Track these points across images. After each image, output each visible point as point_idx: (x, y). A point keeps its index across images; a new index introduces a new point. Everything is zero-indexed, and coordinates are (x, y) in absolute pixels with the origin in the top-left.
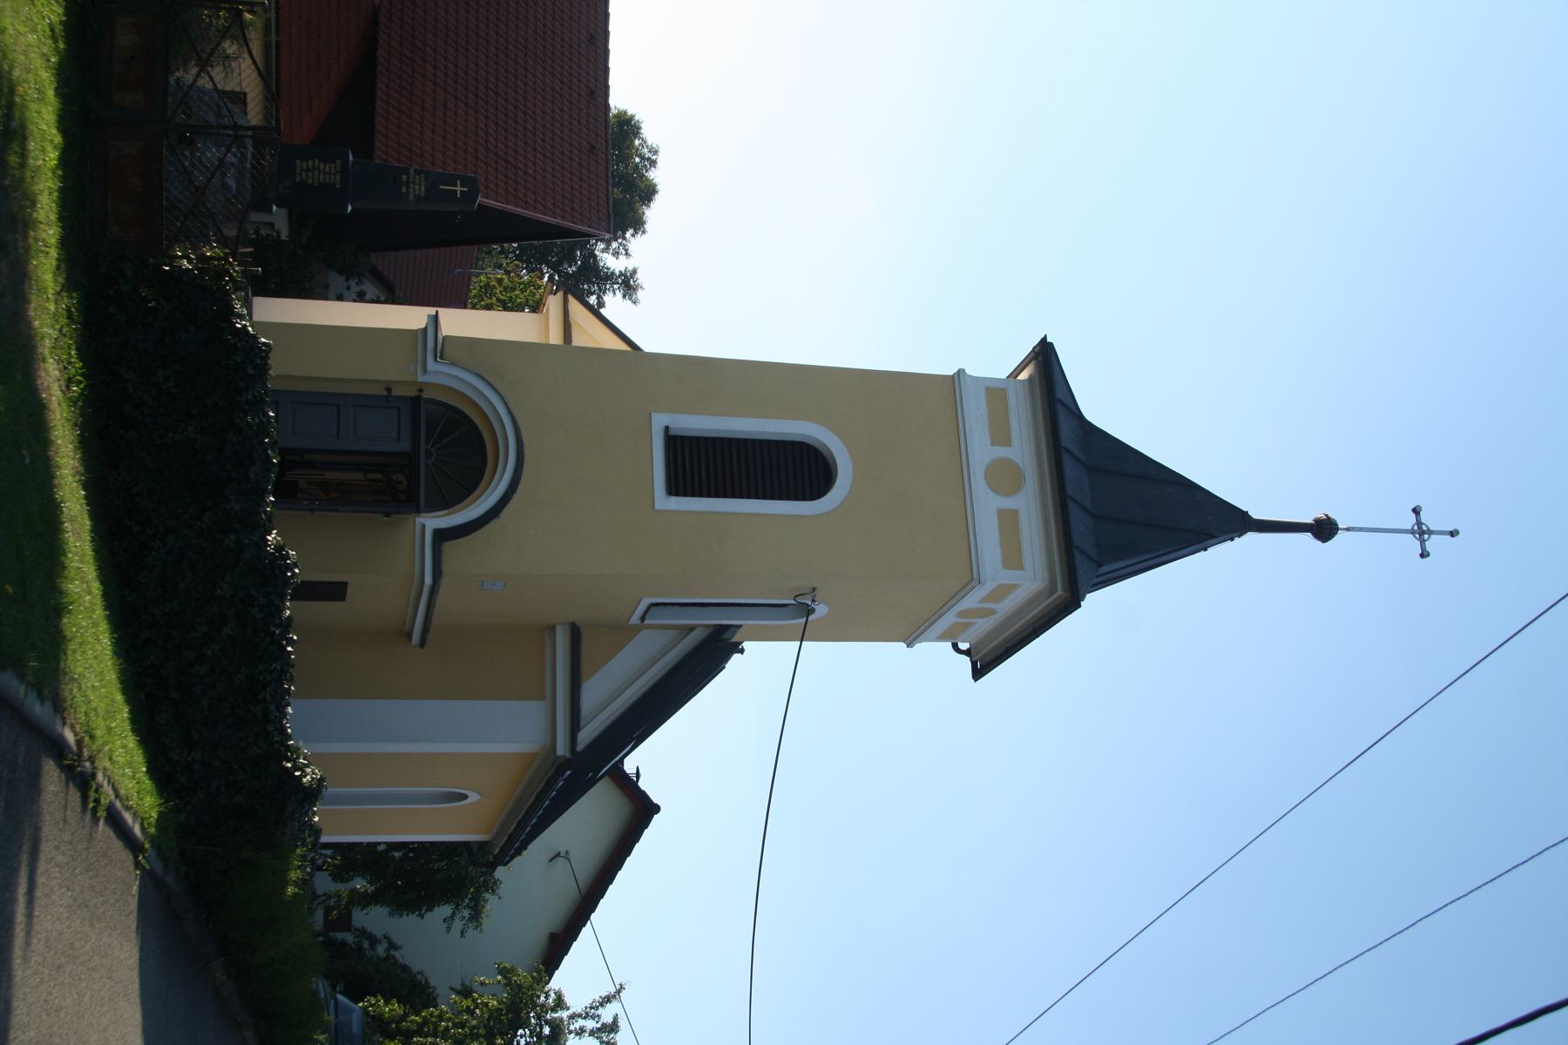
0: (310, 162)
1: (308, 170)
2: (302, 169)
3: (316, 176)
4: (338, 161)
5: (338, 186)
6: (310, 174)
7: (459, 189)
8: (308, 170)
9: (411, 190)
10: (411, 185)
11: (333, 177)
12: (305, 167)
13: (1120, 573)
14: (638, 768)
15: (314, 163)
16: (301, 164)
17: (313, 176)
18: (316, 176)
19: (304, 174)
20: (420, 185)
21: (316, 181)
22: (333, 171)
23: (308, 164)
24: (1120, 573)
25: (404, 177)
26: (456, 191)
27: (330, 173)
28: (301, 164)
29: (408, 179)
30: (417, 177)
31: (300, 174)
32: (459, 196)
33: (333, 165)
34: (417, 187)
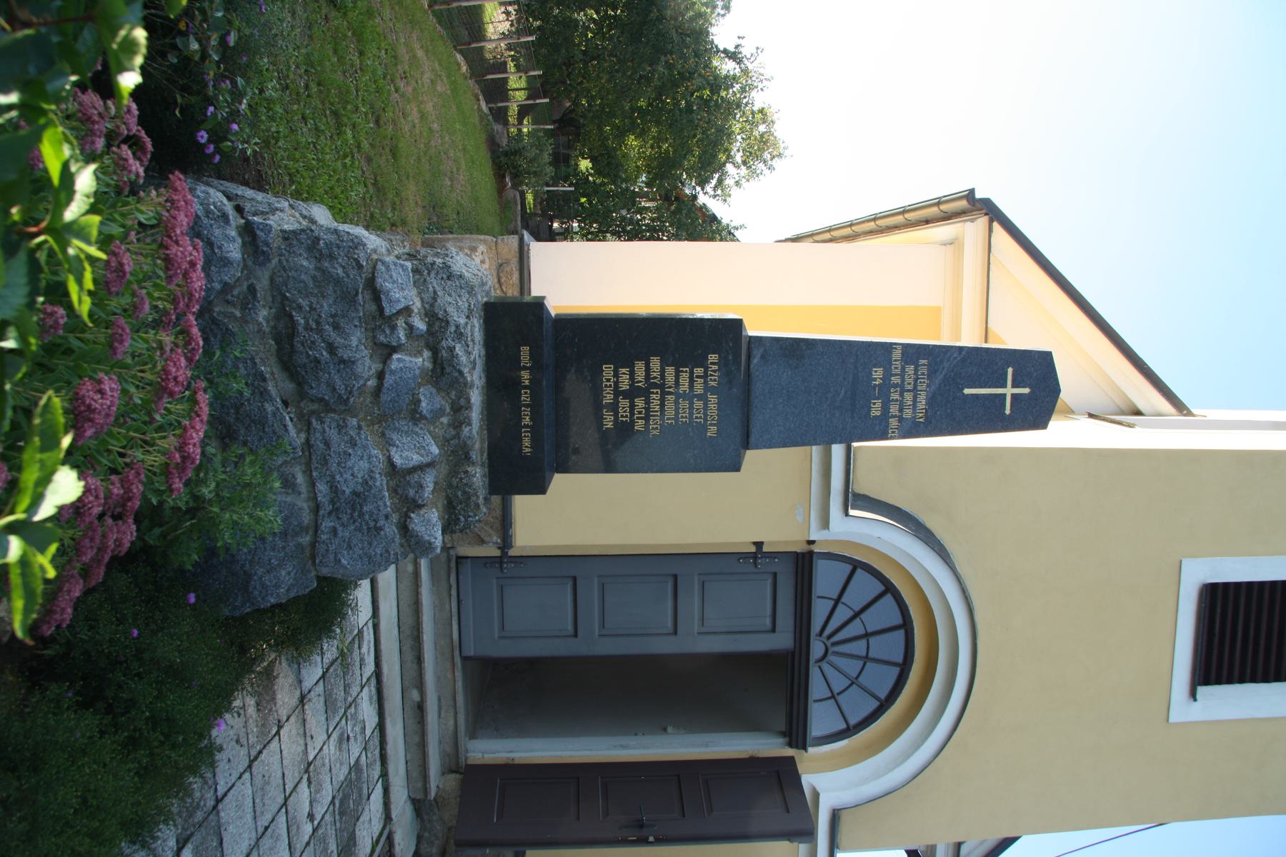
0: (640, 367)
1: (632, 394)
2: (617, 393)
3: (655, 405)
4: (713, 358)
5: (712, 431)
6: (640, 403)
7: (1009, 391)
8: (632, 394)
9: (894, 409)
10: (895, 396)
11: (698, 404)
12: (625, 386)
13: (805, 616)
14: (788, 812)
15: (632, 374)
16: (616, 375)
17: (648, 409)
18: (655, 405)
19: (623, 403)
20: (915, 389)
21: (246, 681)
22: (699, 387)
23: (632, 374)
24: (805, 616)
25: (878, 373)
26: (1004, 386)
27: (690, 397)
28: (616, 375)
29: (888, 375)
30: (910, 369)
31: (614, 407)
32: (1026, 391)
33: (699, 371)
34: (908, 397)
